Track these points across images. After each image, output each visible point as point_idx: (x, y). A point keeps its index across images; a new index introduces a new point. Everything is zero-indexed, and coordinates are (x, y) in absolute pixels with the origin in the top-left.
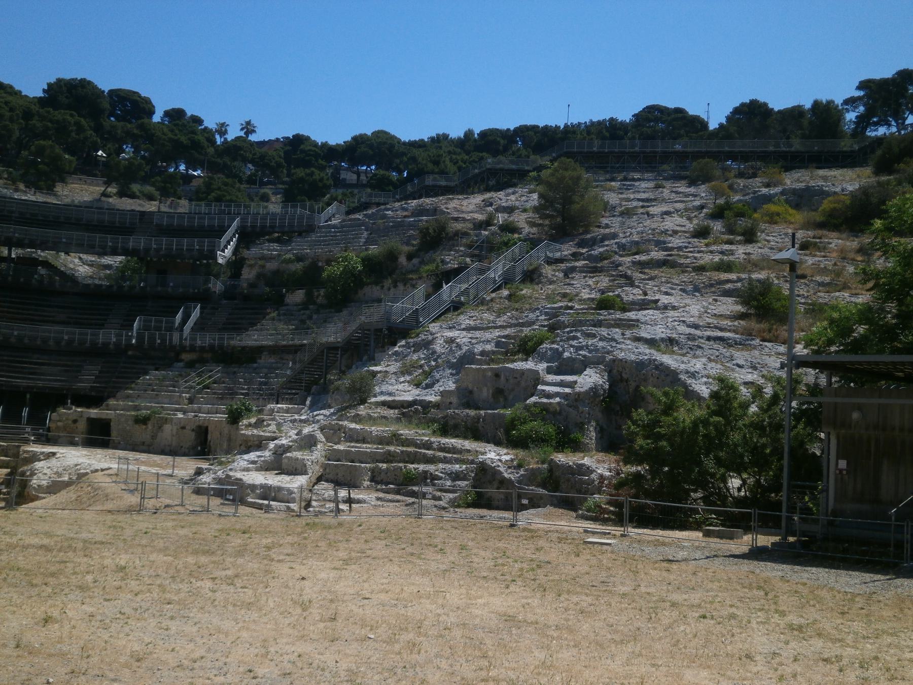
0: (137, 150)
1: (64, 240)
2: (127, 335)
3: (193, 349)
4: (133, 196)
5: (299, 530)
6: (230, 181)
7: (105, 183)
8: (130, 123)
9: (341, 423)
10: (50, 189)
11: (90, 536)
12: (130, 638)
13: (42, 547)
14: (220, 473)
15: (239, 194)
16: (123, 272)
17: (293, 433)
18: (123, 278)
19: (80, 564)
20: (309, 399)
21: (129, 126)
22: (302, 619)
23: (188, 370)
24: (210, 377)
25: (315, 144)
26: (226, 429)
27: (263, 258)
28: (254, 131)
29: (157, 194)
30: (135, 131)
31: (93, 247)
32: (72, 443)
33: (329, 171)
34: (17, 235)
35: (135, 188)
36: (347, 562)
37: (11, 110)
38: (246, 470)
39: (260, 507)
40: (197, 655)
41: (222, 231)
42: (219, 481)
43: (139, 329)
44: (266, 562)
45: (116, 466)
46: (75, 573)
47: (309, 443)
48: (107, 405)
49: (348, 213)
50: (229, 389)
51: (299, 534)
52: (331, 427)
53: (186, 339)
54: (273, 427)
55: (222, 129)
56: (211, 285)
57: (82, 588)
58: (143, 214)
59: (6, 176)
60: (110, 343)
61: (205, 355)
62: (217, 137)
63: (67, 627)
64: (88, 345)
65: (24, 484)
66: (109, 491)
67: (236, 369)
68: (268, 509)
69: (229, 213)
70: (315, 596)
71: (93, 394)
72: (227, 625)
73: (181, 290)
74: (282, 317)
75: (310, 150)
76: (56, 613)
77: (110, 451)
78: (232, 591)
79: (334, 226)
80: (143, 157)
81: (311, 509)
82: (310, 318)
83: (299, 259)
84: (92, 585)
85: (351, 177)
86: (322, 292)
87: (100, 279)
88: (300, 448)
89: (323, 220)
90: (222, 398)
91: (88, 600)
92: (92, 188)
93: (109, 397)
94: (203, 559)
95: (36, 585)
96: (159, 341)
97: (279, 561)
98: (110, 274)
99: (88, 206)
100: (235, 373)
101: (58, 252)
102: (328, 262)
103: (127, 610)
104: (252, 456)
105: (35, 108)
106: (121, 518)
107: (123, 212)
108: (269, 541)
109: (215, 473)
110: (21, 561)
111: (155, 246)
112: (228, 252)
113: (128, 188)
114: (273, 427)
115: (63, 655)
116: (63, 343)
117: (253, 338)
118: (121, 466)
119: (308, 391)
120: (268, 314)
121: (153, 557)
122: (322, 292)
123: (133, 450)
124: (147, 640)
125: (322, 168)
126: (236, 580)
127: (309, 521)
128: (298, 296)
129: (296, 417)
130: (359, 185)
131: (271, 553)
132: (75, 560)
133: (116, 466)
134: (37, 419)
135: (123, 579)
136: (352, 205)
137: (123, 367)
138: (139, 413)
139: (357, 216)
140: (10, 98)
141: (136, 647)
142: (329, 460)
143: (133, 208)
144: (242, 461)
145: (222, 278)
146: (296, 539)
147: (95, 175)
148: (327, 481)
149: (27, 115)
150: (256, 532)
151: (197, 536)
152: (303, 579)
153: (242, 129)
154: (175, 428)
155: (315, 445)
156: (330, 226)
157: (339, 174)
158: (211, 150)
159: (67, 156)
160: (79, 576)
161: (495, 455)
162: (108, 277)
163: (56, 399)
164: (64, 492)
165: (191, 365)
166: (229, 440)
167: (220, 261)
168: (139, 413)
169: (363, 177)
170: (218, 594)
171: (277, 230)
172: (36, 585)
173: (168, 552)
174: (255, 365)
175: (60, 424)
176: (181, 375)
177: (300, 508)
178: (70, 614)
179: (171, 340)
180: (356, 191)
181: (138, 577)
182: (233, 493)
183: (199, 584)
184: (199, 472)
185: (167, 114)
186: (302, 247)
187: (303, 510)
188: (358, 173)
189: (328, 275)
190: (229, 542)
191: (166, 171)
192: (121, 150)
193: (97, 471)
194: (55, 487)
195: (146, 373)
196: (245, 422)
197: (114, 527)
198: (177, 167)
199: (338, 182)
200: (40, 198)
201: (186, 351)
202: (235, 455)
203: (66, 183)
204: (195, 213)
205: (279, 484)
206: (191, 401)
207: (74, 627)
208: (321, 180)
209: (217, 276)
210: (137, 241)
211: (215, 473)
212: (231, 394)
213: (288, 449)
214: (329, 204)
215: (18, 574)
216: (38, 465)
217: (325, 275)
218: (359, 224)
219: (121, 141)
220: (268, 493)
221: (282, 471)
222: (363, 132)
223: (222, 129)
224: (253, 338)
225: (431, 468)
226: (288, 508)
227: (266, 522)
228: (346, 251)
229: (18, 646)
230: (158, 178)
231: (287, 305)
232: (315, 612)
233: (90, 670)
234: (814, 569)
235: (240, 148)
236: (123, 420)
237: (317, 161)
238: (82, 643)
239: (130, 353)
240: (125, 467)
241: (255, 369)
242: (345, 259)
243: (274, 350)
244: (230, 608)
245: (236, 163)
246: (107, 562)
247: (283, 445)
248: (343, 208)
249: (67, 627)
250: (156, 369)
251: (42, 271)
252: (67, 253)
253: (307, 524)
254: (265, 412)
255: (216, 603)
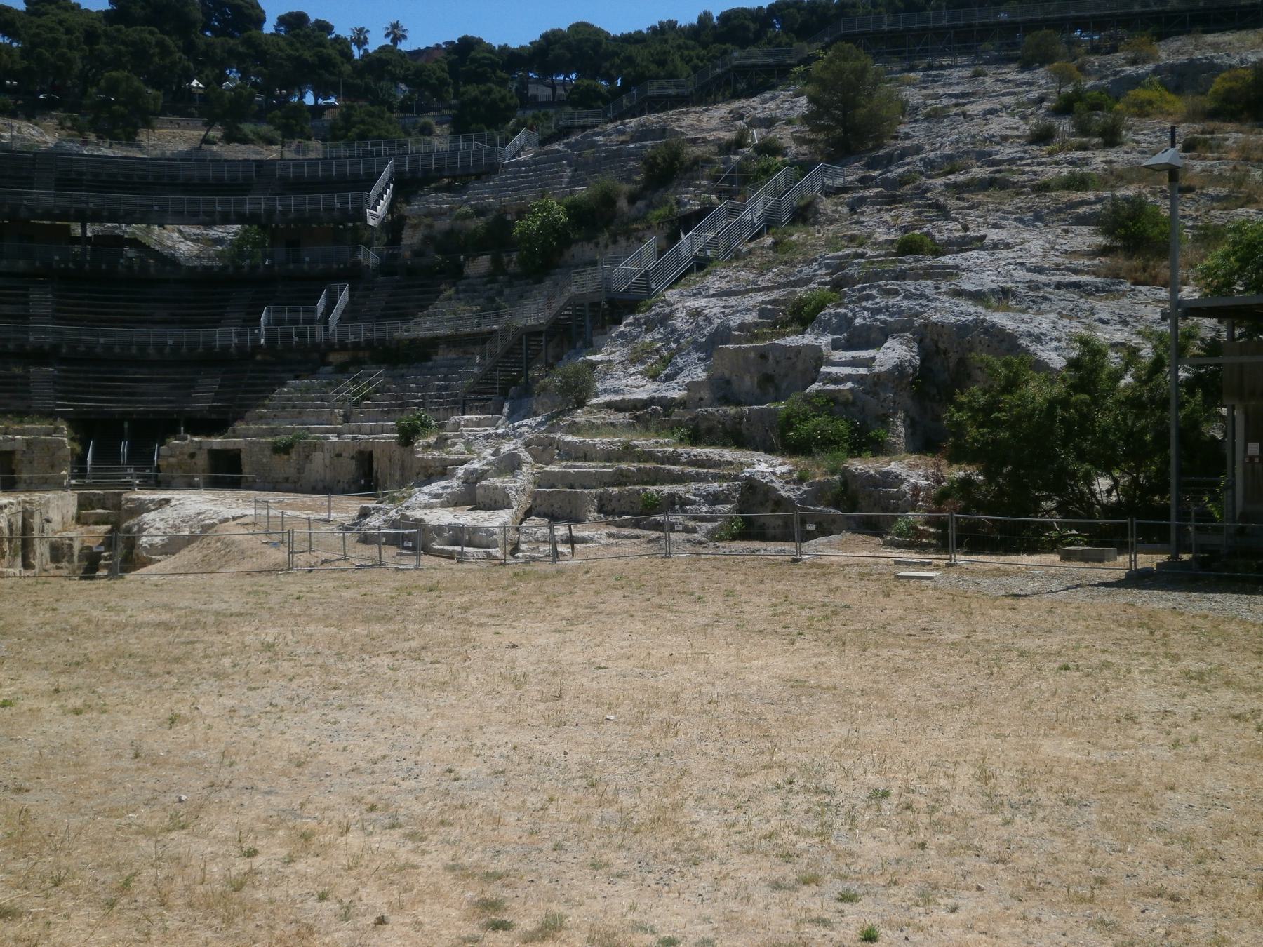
0: (245, 75)
1: (156, 208)
2: (252, 334)
3: (343, 347)
4: (244, 140)
5: (505, 582)
6: (375, 109)
7: (205, 124)
8: (232, 37)
9: (552, 435)
10: (130, 138)
11: (224, 606)
12: (286, 736)
13: (159, 624)
14: (393, 513)
15: (390, 127)
16: (240, 247)
17: (487, 453)
18: (241, 255)
19: (212, 644)
20: (507, 405)
21: (232, 42)
22: (515, 700)
23: (339, 376)
24: (370, 384)
25: (490, 49)
26: (398, 452)
27: (430, 214)
28: (404, 37)
29: (277, 134)
30: (241, 49)
31: (196, 214)
32: (191, 486)
33: (513, 86)
34: (91, 205)
35: (247, 128)
36: (571, 621)
37: (69, 31)
38: (428, 506)
39: (449, 556)
40: (377, 753)
41: (371, 180)
42: (393, 524)
43: (268, 324)
44: (462, 627)
45: (252, 512)
46: (205, 657)
47: (510, 465)
48: (234, 431)
49: (543, 143)
50: (397, 398)
51: (505, 588)
52: (539, 442)
53: (333, 334)
54: (460, 447)
55: (360, 38)
56: (361, 257)
57: (217, 675)
58: (260, 163)
59: (69, 124)
60: (229, 347)
61: (361, 354)
62: (354, 48)
63: (201, 727)
64: (200, 350)
65: (131, 544)
66: (245, 545)
67: (404, 371)
68: (461, 558)
69: (379, 155)
70: (531, 668)
71: (213, 416)
72: (416, 713)
73: (321, 266)
74: (461, 296)
75: (484, 58)
76: (184, 710)
77: (243, 493)
78: (419, 668)
79: (524, 163)
80: (254, 85)
81: (520, 554)
82: (500, 293)
83: (480, 212)
84: (230, 671)
85: (543, 92)
86: (514, 256)
87: (209, 258)
88: (499, 473)
89: (508, 155)
90: (388, 411)
91: (226, 691)
92: (188, 133)
93: (235, 420)
94: (378, 629)
95: (156, 675)
96: (296, 339)
97: (480, 625)
98: (223, 251)
99: (185, 158)
100: (403, 376)
101: (149, 225)
102: (520, 215)
103: (279, 701)
104: (435, 487)
105: (101, 27)
106: (263, 580)
107: (232, 164)
108: (465, 599)
109: (386, 514)
110: (134, 645)
111: (280, 208)
112: (381, 209)
113: (238, 129)
114: (460, 447)
115: (197, 764)
116: (168, 350)
117: (424, 327)
118: (259, 512)
119: (504, 395)
120: (442, 292)
121: (311, 628)
122: (514, 256)
123: (274, 489)
124: (309, 738)
125: (502, 83)
126: (423, 654)
127: (517, 570)
128: (482, 264)
129: (491, 431)
130: (555, 103)
131: (468, 615)
132: (206, 638)
133: (252, 512)
134: (141, 456)
135: (272, 660)
136: (549, 132)
137: (251, 377)
138: (278, 438)
139: (555, 146)
140: (65, 15)
141: (295, 748)
142: (540, 487)
143: (246, 156)
144: (422, 495)
145: (376, 245)
146: (501, 595)
147: (191, 115)
148: (538, 515)
149: (91, 36)
150: (447, 589)
151: (368, 598)
152: (514, 646)
153: (387, 35)
154: (328, 456)
155: (519, 467)
156: (518, 164)
157: (527, 89)
158: (347, 68)
159: (149, 91)
160: (213, 660)
161: (766, 467)
162: (220, 255)
163: (164, 427)
164: (185, 552)
165: (342, 369)
166: (403, 468)
167: (371, 222)
168: (278, 438)
169: (560, 91)
170: (400, 673)
171: (446, 174)
172: (156, 675)
173: (330, 621)
174: (430, 364)
175: (172, 460)
176: (330, 384)
177: (505, 554)
178: (204, 710)
179: (313, 336)
180: (551, 111)
181: (292, 657)
182: (412, 539)
183: (374, 661)
184: (365, 513)
185: (282, 20)
186: (482, 195)
187: (508, 556)
188: (553, 86)
189: (521, 232)
190: (411, 603)
191: (288, 101)
192: (223, 78)
193: (227, 520)
194: (173, 545)
195: (283, 384)
196: (422, 442)
197: (256, 592)
198: (302, 96)
199: (527, 101)
200: (119, 151)
201: (336, 350)
202: (412, 487)
203: (153, 129)
204: (332, 158)
205: (474, 523)
206: (346, 418)
207: (210, 727)
208: (503, 99)
209: (368, 244)
210: (256, 203)
211: (386, 514)
212: (400, 405)
213: (483, 475)
214: (515, 133)
215: (130, 662)
216: (148, 517)
217: (516, 232)
218: (557, 158)
219: (222, 65)
220: (460, 536)
221: (478, 506)
222: (556, 27)
223: (360, 38)
224: (424, 327)
225: (679, 489)
226: (489, 554)
227: (459, 575)
228: (542, 197)
229: (137, 756)
230: (278, 113)
231: (468, 277)
232: (532, 689)
233: (235, 782)
234: (1218, 596)
235: (388, 62)
236: (256, 449)
237: (494, 72)
238: (222, 747)
239: (259, 357)
240: (264, 512)
241: (431, 368)
242: (543, 208)
243: (458, 342)
244: (418, 690)
245: (383, 84)
246: (249, 639)
247: (475, 470)
248: (535, 136)
249: (201, 727)
250: (296, 378)
251: (129, 252)
252: (161, 226)
253: (516, 575)
254: (448, 427)
255: (399, 685)
